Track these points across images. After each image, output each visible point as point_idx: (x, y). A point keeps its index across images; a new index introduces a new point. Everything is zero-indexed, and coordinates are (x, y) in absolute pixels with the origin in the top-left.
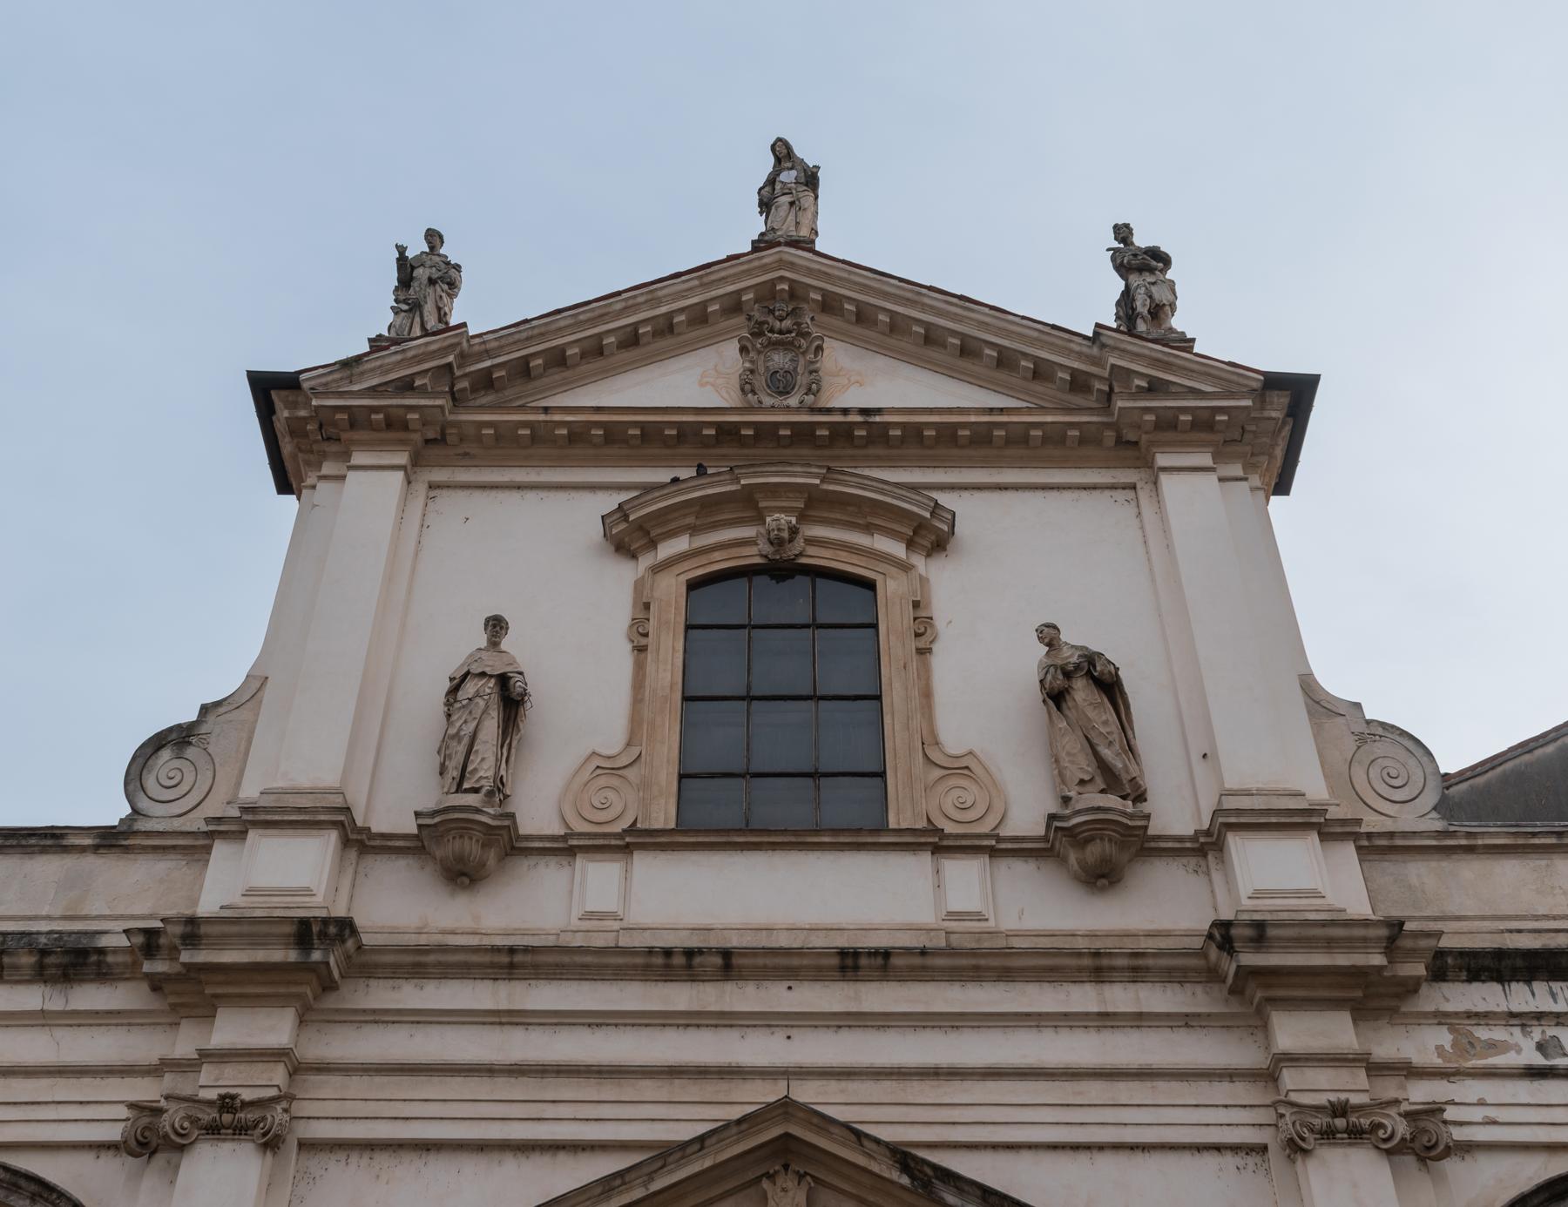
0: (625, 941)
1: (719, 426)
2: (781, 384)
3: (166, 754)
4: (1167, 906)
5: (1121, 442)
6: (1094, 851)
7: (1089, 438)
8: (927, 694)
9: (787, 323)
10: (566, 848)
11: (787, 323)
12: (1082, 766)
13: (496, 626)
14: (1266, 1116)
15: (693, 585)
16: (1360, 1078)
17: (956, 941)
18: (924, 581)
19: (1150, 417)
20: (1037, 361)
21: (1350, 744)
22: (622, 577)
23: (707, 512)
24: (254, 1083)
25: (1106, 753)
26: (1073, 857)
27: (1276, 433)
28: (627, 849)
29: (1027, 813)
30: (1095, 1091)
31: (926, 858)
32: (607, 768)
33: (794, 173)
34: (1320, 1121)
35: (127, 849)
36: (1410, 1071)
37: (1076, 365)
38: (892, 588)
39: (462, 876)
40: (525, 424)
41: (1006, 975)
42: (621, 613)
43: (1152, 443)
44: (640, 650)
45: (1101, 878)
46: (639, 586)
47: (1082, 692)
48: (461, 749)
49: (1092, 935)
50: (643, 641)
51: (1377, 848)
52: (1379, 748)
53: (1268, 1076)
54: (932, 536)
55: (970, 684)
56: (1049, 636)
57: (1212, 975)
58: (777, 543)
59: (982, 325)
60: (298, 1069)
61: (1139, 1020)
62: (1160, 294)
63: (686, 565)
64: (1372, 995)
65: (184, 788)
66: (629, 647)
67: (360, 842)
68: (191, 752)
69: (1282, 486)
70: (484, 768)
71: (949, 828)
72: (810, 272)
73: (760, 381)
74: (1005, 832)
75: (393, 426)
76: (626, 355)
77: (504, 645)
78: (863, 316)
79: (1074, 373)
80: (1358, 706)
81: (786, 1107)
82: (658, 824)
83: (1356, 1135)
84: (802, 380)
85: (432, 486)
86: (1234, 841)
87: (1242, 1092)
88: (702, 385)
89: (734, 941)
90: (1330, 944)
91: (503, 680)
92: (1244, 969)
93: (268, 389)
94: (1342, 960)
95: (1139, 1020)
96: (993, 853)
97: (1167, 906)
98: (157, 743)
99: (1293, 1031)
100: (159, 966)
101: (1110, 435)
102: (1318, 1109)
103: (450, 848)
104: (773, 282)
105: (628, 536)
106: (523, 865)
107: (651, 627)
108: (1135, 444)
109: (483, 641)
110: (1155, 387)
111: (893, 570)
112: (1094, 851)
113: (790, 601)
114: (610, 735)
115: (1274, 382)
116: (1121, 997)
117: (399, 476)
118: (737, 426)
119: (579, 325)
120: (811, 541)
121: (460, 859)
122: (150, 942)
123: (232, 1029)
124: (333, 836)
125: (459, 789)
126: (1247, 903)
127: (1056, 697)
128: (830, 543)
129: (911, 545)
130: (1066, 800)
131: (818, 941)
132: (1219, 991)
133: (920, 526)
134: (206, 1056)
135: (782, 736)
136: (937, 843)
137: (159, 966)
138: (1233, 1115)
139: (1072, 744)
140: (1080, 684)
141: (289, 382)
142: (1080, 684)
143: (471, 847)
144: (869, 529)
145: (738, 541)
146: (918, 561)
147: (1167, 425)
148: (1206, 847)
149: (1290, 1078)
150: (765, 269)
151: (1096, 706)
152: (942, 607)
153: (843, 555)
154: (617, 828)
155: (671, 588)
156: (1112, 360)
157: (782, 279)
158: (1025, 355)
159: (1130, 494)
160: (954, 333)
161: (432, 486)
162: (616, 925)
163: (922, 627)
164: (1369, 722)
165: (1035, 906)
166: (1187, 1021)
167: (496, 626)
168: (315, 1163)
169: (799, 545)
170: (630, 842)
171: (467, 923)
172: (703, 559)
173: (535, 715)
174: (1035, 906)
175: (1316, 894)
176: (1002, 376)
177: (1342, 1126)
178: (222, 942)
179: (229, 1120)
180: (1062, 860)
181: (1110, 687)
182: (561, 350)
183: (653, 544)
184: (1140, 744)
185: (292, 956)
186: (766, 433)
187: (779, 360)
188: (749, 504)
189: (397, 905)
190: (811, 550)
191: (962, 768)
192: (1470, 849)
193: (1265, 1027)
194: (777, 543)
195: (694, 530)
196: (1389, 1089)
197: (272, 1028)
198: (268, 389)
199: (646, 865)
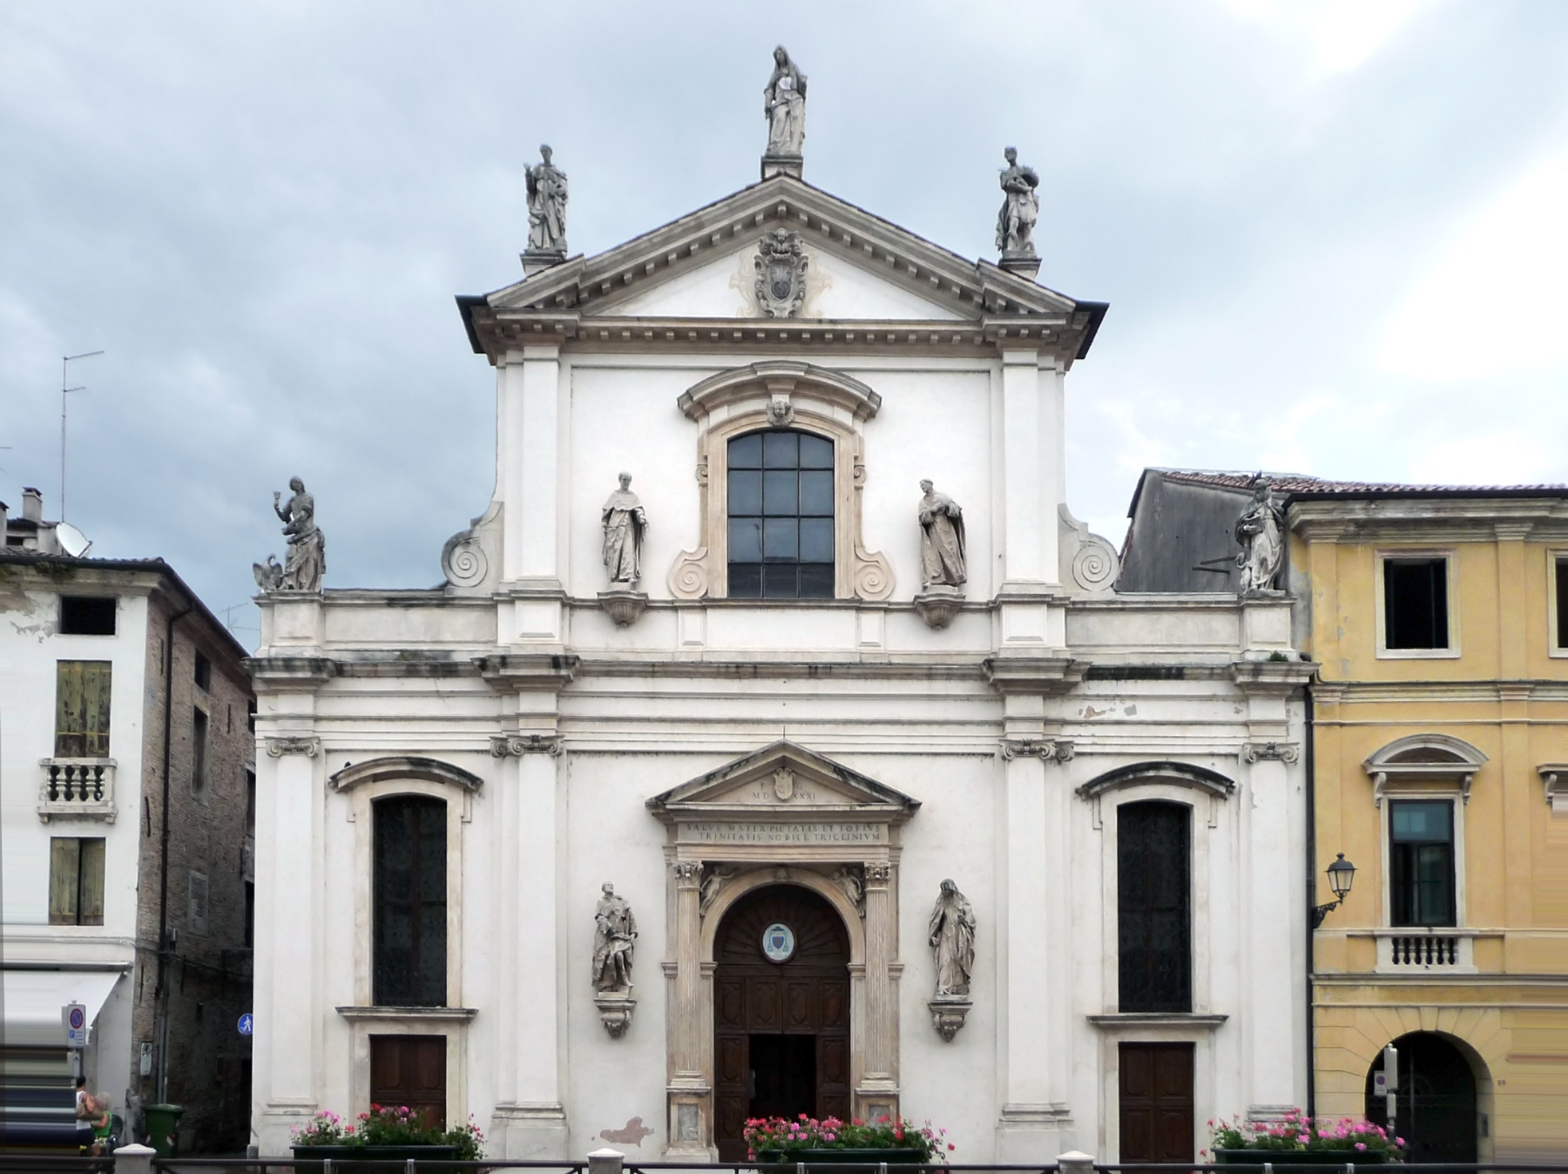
0: (706, 659)
1: (744, 331)
2: (781, 292)
3: (458, 550)
4: (968, 640)
5: (985, 343)
6: (936, 614)
7: (967, 340)
8: (859, 516)
9: (785, 246)
10: (674, 607)
11: (785, 246)
12: (934, 569)
13: (625, 480)
14: (995, 741)
15: (730, 441)
16: (1040, 727)
17: (867, 660)
18: (861, 440)
19: (1004, 331)
20: (941, 278)
21: (1077, 546)
22: (691, 434)
23: (738, 392)
24: (546, 729)
25: (948, 562)
26: (925, 615)
27: (1076, 338)
28: (704, 608)
29: (906, 589)
30: (935, 730)
31: (853, 613)
32: (691, 562)
33: (789, 79)
34: (1017, 748)
35: (454, 606)
36: (1064, 722)
37: (964, 283)
38: (843, 445)
39: (623, 622)
40: (627, 329)
41: (887, 676)
42: (690, 462)
43: (1003, 346)
44: (704, 486)
45: (939, 625)
46: (701, 444)
47: (940, 525)
48: (617, 556)
49: (930, 655)
50: (705, 480)
51: (1074, 609)
52: (1091, 551)
53: (1000, 724)
54: (866, 409)
55: (878, 524)
56: (927, 487)
57: (983, 678)
58: (779, 416)
59: (909, 249)
60: (561, 720)
61: (946, 697)
62: (1028, 213)
63: (727, 429)
64: (1054, 690)
65: (473, 570)
66: (697, 483)
67: (570, 605)
68: (472, 548)
69: (1081, 355)
70: (628, 572)
71: (866, 597)
72: (800, 198)
73: (767, 290)
74: (893, 599)
75: (547, 334)
76: (684, 263)
77: (630, 488)
78: (835, 234)
79: (962, 289)
80: (1086, 525)
81: (784, 746)
82: (717, 596)
83: (1033, 753)
84: (794, 288)
85: (574, 367)
86: (1005, 610)
87: (987, 730)
88: (732, 286)
89: (759, 659)
90: (1038, 669)
91: (633, 514)
92: (996, 678)
93: (471, 308)
94: (1043, 676)
95: (946, 697)
96: (886, 610)
97: (968, 640)
98: (452, 546)
99: (1018, 706)
100: (489, 675)
101: (979, 339)
102: (1018, 742)
103: (618, 610)
104: (776, 205)
105: (694, 408)
106: (654, 615)
107: (709, 470)
108: (993, 344)
109: (618, 486)
110: (1011, 309)
111: (845, 433)
112: (936, 614)
113: (782, 452)
114: (691, 543)
115: (1081, 307)
116: (940, 687)
117: (555, 365)
118: (756, 331)
119: (654, 246)
120: (798, 412)
121: (622, 615)
122: (483, 664)
123: (530, 703)
124: (558, 605)
125: (616, 579)
126: (1006, 643)
127: (927, 526)
128: (810, 412)
129: (855, 414)
130: (925, 588)
131: (799, 659)
132: (985, 684)
133: (861, 405)
134: (518, 716)
135: (780, 541)
136: (858, 606)
137: (489, 675)
138: (984, 740)
139: (932, 556)
140: (942, 520)
141: (482, 302)
142: (942, 520)
143: (627, 610)
144: (831, 403)
145: (753, 412)
146: (858, 426)
147: (1015, 338)
148: (992, 609)
149: (1009, 727)
150: (772, 195)
151: (946, 533)
152: (871, 463)
153: (816, 422)
154: (696, 597)
155: (719, 444)
156: (987, 285)
157: (782, 202)
158: (934, 274)
159: (985, 376)
160: (891, 254)
161: (574, 367)
162: (700, 648)
163: (859, 470)
164: (1091, 535)
165: (902, 639)
166: (968, 698)
167: (625, 480)
168: (574, 758)
169: (792, 415)
170: (706, 604)
171: (628, 646)
172: (736, 425)
173: (650, 535)
174: (902, 639)
175: (1039, 639)
176: (917, 284)
177: (1027, 749)
178: (517, 666)
179: (537, 745)
180: (920, 615)
181: (956, 521)
182: (644, 265)
183: (707, 413)
184: (968, 552)
185: (552, 672)
186: (772, 336)
187: (780, 274)
188: (762, 387)
189: (593, 638)
190: (798, 419)
191: (875, 562)
192: (1122, 610)
193: (1003, 700)
194: (779, 416)
195: (730, 403)
196: (1053, 730)
197: (545, 703)
198: (471, 308)
199: (713, 615)
